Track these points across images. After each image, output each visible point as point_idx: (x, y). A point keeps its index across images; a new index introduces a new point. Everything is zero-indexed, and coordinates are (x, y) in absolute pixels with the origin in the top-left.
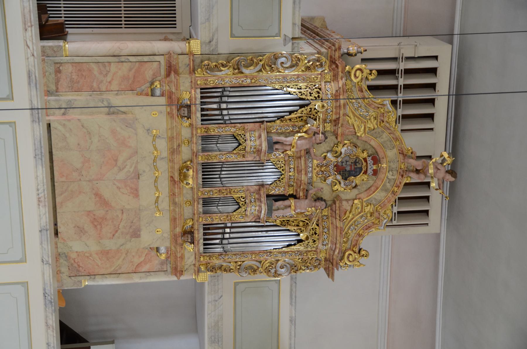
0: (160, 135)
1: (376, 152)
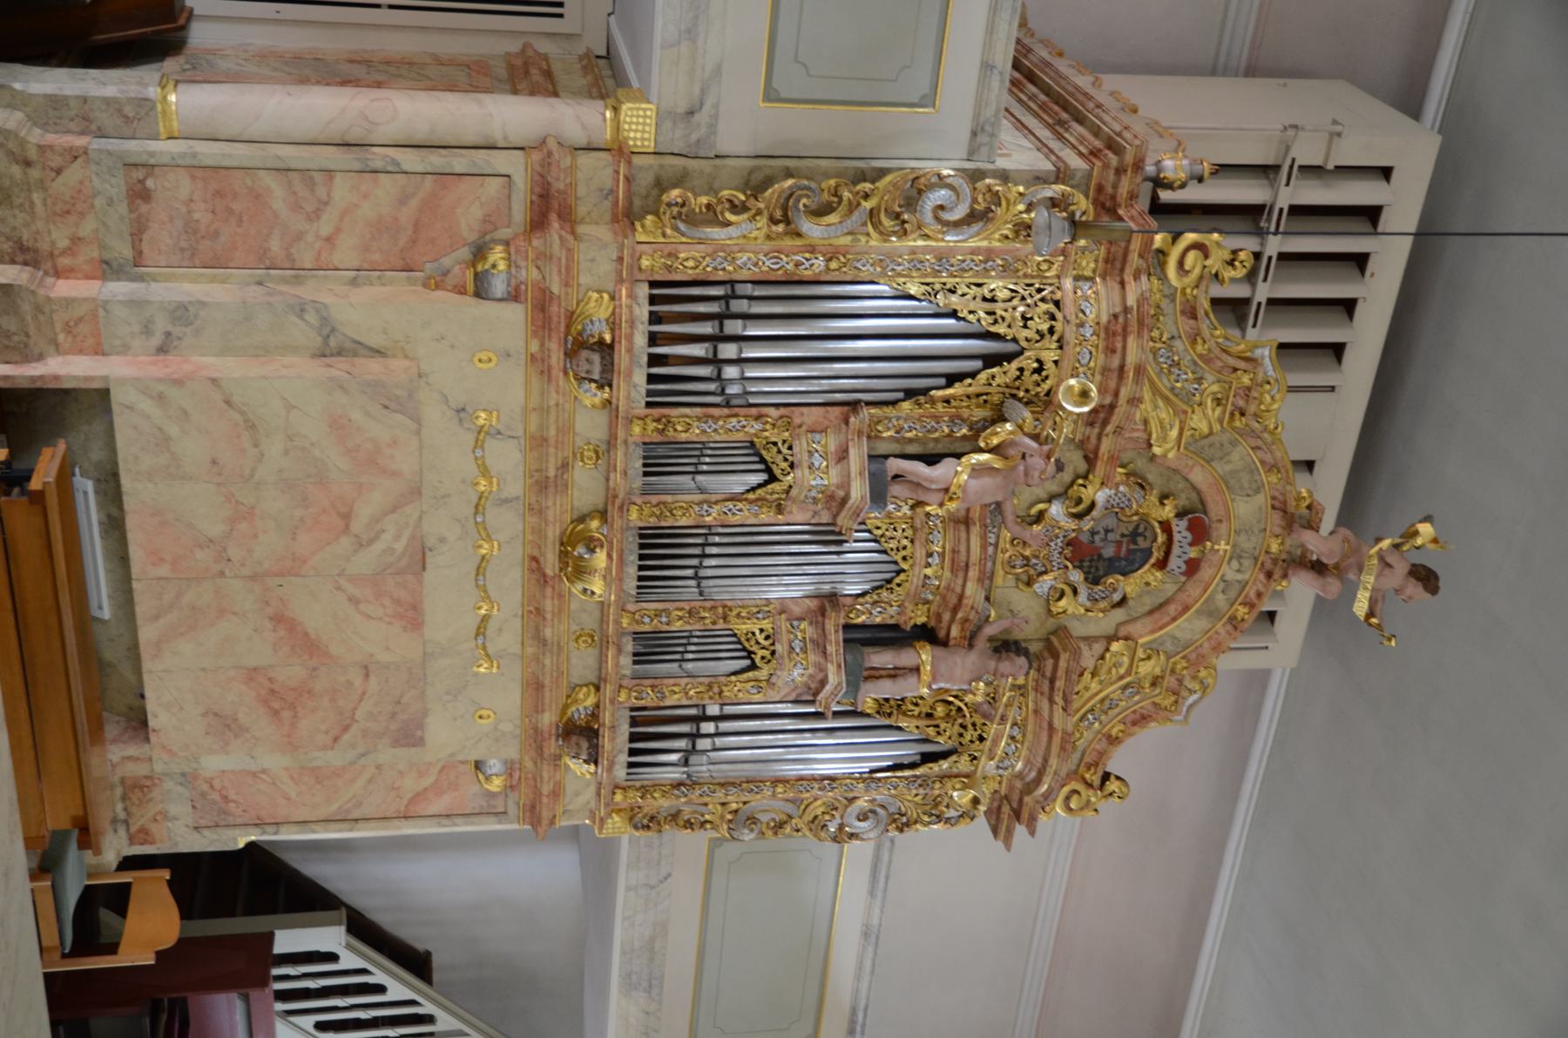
0: (500, 427)
1: (1202, 502)
